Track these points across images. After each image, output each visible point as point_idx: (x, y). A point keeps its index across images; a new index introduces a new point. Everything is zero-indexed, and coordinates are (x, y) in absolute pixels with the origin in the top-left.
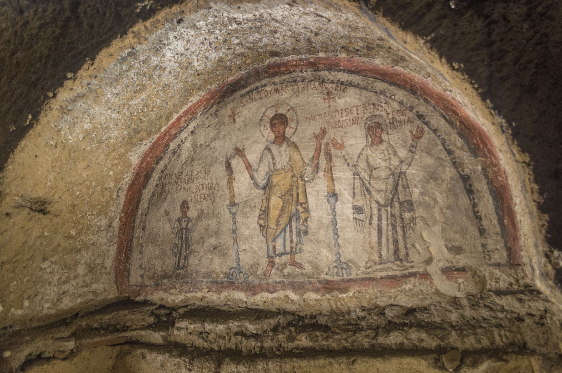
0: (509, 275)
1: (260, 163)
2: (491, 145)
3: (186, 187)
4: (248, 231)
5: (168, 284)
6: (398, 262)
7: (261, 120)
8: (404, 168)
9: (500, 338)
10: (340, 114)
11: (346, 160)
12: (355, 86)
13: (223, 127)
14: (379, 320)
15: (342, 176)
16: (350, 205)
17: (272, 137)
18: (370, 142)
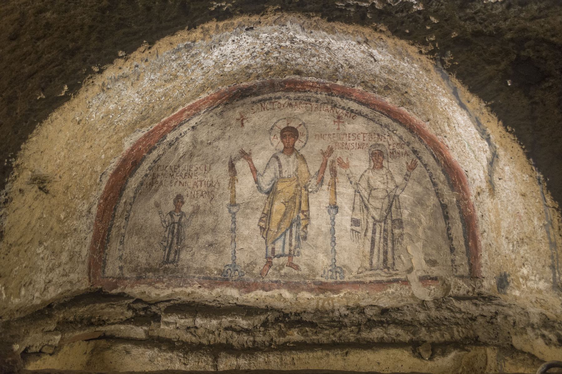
0: (469, 285)
1: (266, 169)
2: (465, 183)
3: (183, 181)
4: (248, 231)
5: (154, 278)
6: (386, 270)
7: (272, 129)
8: (398, 192)
9: (458, 333)
10: (348, 138)
11: (349, 178)
12: (364, 116)
13: (229, 128)
14: (360, 318)
15: (345, 192)
16: (349, 218)
17: (281, 146)
18: (372, 166)
